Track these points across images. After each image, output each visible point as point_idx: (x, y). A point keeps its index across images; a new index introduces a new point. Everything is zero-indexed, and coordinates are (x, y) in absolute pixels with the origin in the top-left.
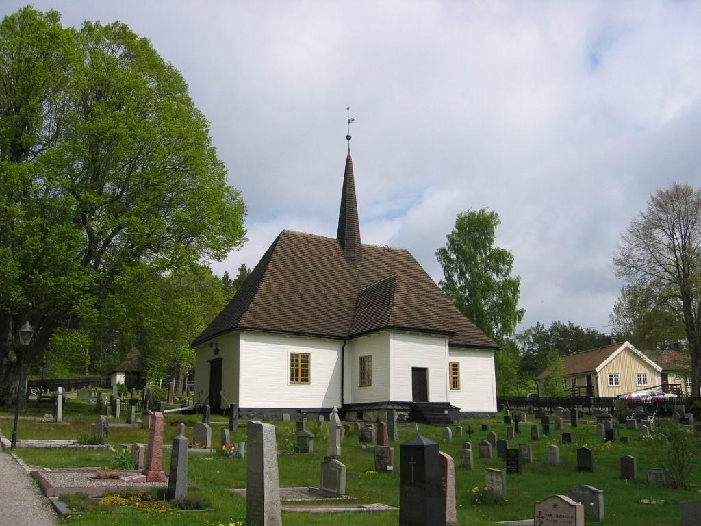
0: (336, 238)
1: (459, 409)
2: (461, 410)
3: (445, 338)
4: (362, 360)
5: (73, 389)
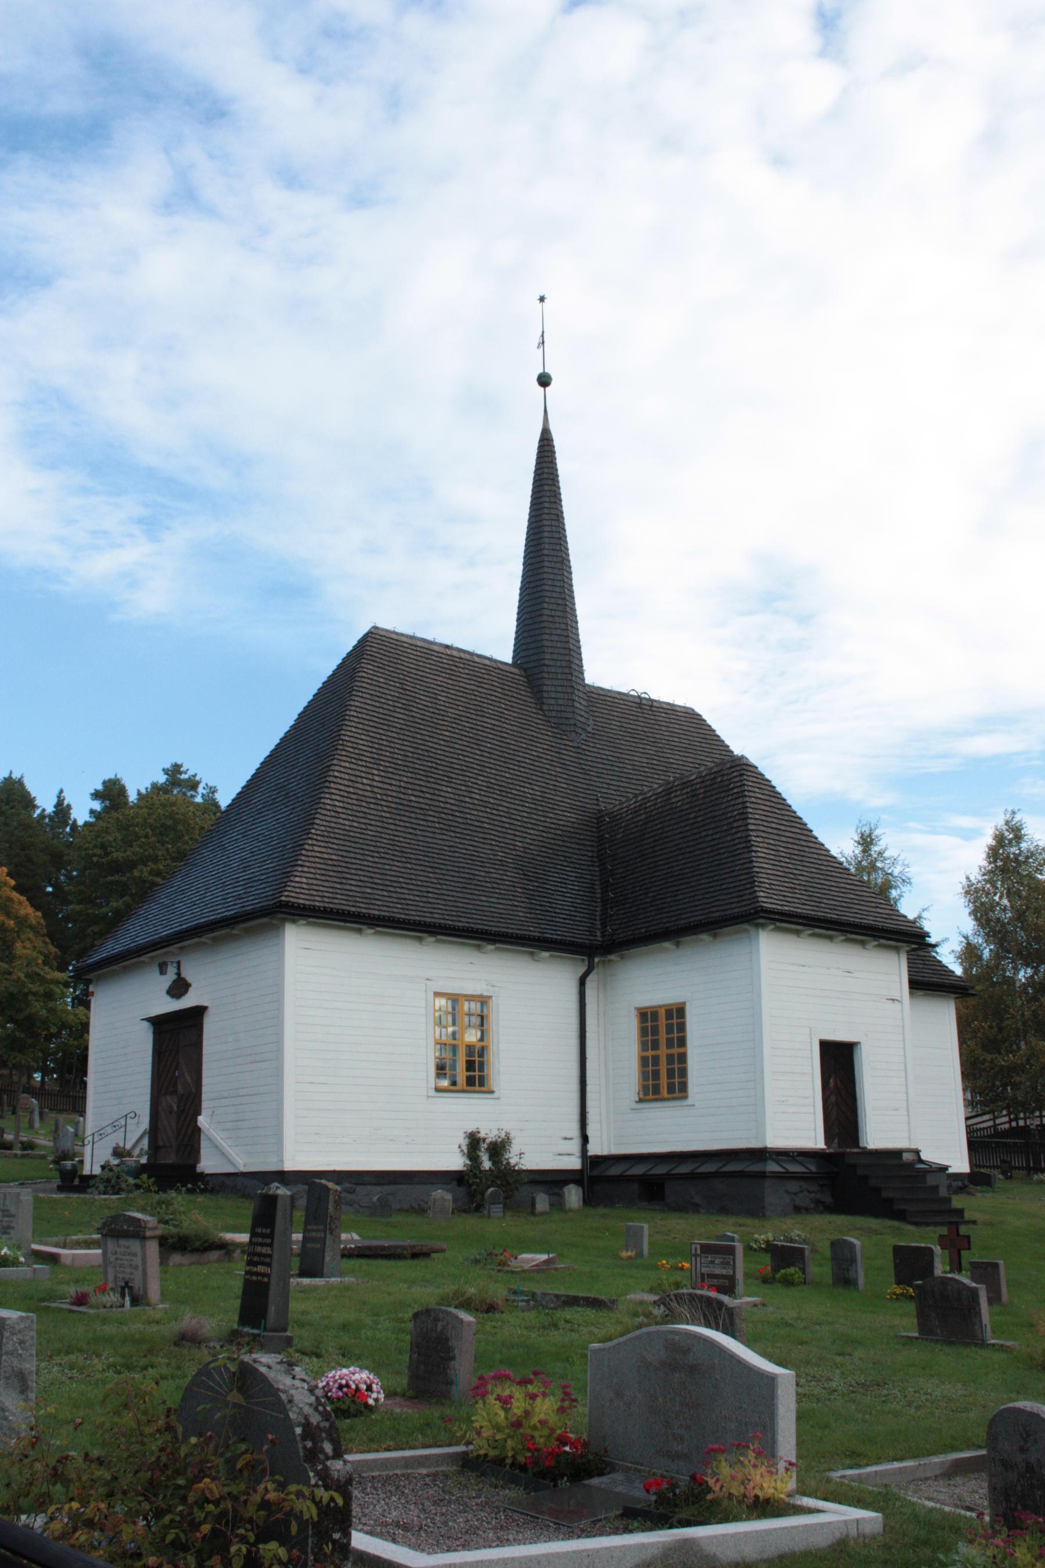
0: (509, 660)
1: (946, 1168)
2: (950, 1171)
3: (897, 949)
4: (647, 1017)
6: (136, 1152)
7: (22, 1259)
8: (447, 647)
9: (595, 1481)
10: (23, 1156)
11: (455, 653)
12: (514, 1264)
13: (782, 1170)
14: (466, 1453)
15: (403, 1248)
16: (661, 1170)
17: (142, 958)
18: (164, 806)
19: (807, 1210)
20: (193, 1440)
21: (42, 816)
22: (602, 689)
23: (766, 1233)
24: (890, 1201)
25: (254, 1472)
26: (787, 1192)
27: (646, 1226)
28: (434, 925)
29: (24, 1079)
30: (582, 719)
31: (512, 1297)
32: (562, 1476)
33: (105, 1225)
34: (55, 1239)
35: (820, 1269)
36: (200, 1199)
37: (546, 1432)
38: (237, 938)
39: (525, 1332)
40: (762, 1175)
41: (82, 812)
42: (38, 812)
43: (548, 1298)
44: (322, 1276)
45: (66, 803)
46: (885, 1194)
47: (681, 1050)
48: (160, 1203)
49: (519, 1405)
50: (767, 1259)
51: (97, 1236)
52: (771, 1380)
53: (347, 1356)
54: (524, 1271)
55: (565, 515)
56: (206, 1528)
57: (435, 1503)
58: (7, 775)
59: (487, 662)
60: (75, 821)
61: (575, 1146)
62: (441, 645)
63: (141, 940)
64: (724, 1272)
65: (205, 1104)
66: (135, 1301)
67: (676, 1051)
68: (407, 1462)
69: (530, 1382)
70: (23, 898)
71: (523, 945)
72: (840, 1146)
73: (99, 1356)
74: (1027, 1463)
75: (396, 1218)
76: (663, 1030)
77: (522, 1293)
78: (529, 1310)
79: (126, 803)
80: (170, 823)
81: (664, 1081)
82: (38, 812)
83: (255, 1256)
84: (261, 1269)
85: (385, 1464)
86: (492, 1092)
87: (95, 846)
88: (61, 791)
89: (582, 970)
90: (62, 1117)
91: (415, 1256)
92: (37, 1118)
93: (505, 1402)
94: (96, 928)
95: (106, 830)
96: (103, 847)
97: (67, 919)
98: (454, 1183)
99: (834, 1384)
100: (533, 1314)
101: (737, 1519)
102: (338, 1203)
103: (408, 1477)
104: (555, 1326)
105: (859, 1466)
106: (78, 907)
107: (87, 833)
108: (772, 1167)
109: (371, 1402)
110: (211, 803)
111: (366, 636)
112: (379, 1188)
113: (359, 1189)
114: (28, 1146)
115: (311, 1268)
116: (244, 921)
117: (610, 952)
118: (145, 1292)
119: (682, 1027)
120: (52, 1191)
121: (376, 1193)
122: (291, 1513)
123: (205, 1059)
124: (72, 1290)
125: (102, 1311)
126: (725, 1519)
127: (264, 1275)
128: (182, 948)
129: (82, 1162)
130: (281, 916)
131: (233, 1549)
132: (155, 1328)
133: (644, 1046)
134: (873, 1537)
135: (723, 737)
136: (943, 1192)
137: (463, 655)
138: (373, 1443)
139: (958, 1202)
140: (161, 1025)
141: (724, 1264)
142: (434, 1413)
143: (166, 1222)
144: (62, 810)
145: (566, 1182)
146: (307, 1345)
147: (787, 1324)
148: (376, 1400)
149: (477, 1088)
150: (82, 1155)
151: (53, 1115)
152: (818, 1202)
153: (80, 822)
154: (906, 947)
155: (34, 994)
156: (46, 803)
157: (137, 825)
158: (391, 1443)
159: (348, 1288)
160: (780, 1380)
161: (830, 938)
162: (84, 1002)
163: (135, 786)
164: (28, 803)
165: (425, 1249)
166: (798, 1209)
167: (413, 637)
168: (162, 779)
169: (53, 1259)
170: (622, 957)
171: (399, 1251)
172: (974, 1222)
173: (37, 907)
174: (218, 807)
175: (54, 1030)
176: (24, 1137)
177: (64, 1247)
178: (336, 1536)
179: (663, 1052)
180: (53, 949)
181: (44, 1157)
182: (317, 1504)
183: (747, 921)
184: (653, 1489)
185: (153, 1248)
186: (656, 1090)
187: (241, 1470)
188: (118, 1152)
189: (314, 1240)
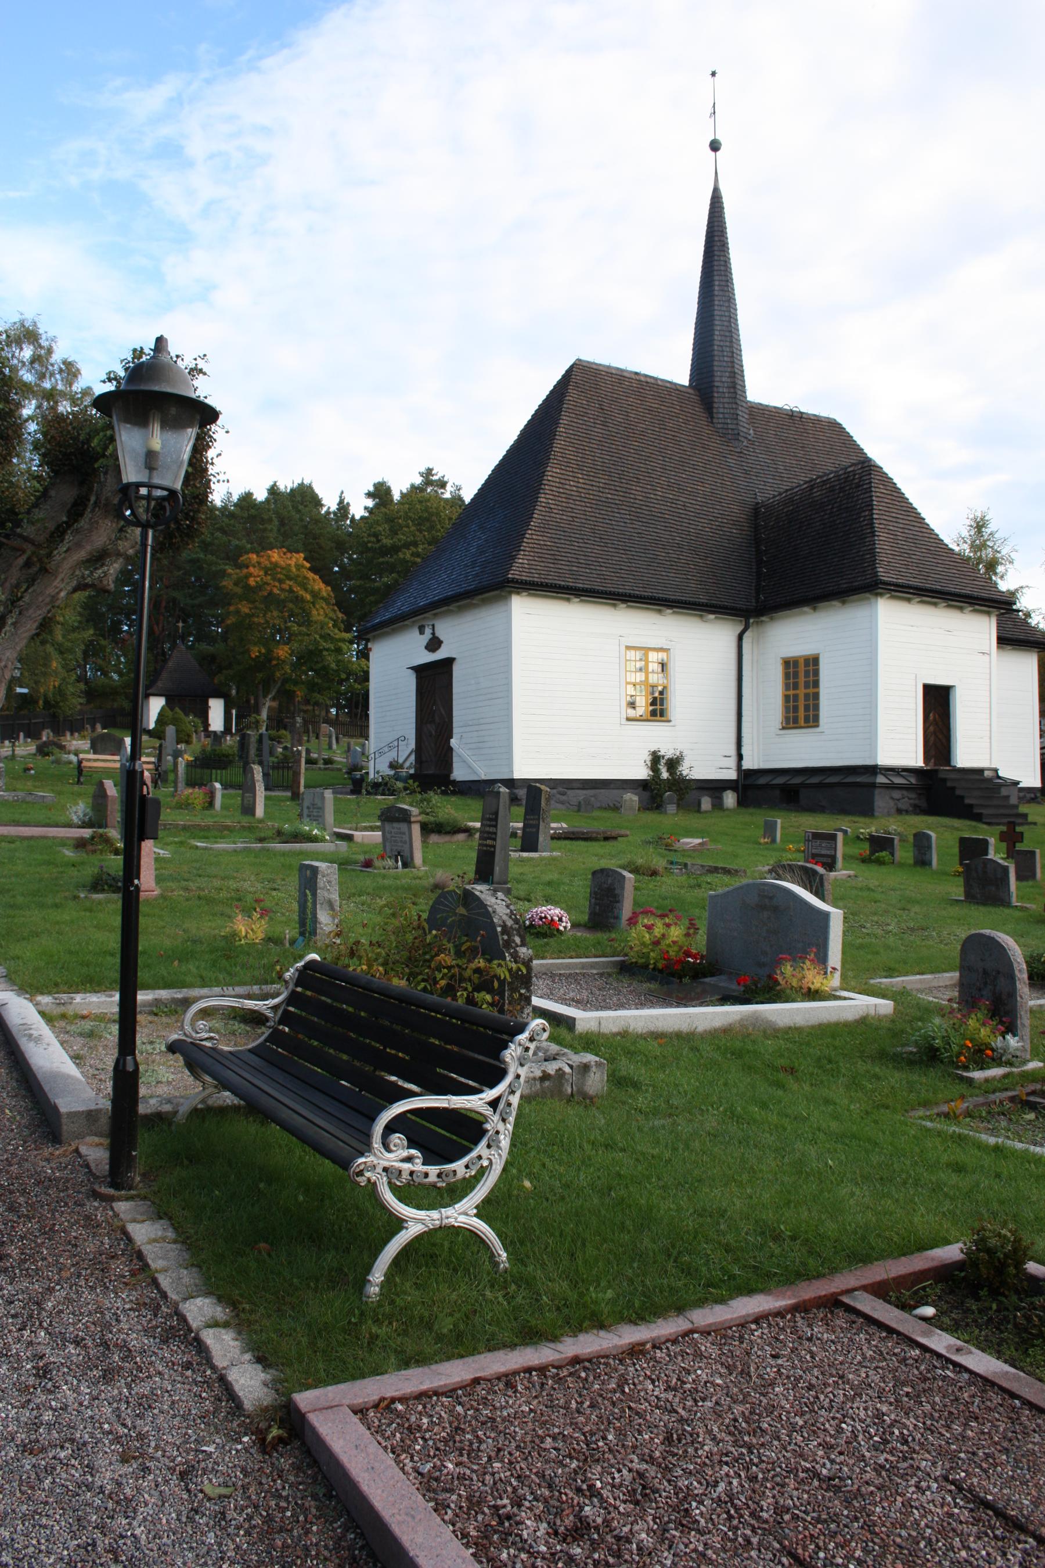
0: (687, 384)
1: (1018, 783)
2: (1021, 785)
3: (988, 613)
4: (790, 666)
5: (68, 734)
6: (407, 764)
7: (327, 838)
8: (636, 373)
9: (707, 980)
10: (326, 769)
11: (643, 379)
12: (677, 846)
13: (888, 781)
14: (624, 961)
15: (598, 833)
16: (797, 780)
17: (406, 623)
18: (420, 502)
19: (907, 812)
20: (434, 932)
21: (328, 513)
22: (761, 404)
23: (869, 828)
24: (971, 806)
25: (473, 953)
26: (892, 798)
27: (779, 821)
28: (625, 595)
29: (323, 713)
30: (745, 430)
31: (669, 866)
32: (685, 976)
33: (382, 814)
34: (349, 826)
35: (904, 853)
36: (453, 799)
37: (676, 948)
38: (475, 606)
39: (677, 889)
40: (873, 785)
41: (359, 507)
42: (325, 509)
43: (696, 867)
44: (536, 851)
45: (346, 502)
46: (967, 801)
47: (815, 690)
48: (422, 801)
49: (658, 931)
50: (866, 846)
51: (378, 824)
52: (826, 916)
53: (548, 900)
54: (684, 850)
55: (732, 261)
56: (443, 983)
57: (600, 990)
58: (300, 482)
59: (668, 385)
60: (353, 516)
61: (732, 762)
62: (631, 372)
63: (406, 608)
64: (828, 852)
65: (455, 731)
66: (405, 865)
67: (811, 690)
68: (583, 966)
69: (666, 915)
70: (317, 577)
71: (694, 609)
72: (935, 765)
73: (381, 898)
74: (984, 970)
75: (596, 813)
76: (802, 675)
77: (677, 863)
78: (682, 875)
79: (392, 500)
80: (425, 515)
81: (801, 713)
82: (325, 509)
83: (489, 833)
84: (489, 842)
85: (568, 966)
86: (669, 721)
87: (369, 535)
88: (342, 493)
89: (740, 628)
90: (352, 741)
91: (606, 839)
92: (334, 741)
93: (649, 928)
94: (372, 598)
95: (377, 523)
96: (376, 535)
97: (350, 591)
98: (641, 789)
99: (890, 928)
100: (685, 877)
101: (793, 1001)
102: (548, 800)
103: (584, 975)
104: (699, 886)
105: (892, 977)
106: (358, 583)
107: (362, 525)
108: (881, 779)
109: (561, 928)
110: (457, 499)
111: (572, 367)
112: (584, 792)
113: (569, 792)
114: (328, 762)
115: (529, 843)
116: (481, 594)
117: (762, 615)
118: (412, 858)
119: (816, 673)
120: (347, 794)
121: (582, 794)
122: (495, 976)
123: (454, 697)
124: (361, 858)
125: (383, 871)
126: (787, 1001)
127: (491, 846)
128: (435, 615)
129: (367, 773)
130: (508, 589)
131: (459, 994)
132: (418, 881)
133: (787, 686)
134: (886, 1016)
135: (859, 442)
136: (1013, 800)
137: (649, 380)
138: (560, 954)
139: (1023, 809)
140: (421, 671)
141: (829, 849)
142: (602, 936)
143: (427, 814)
144: (343, 508)
145: (725, 789)
146: (522, 894)
147: (869, 889)
148: (565, 927)
149: (658, 718)
150: (368, 768)
151: (346, 739)
152: (915, 806)
153: (357, 517)
154: (996, 612)
155: (327, 650)
156: (330, 503)
157: (400, 518)
158: (573, 954)
159: (554, 859)
160: (832, 916)
161: (935, 604)
162: (364, 654)
163: (397, 491)
164: (317, 502)
165: (613, 835)
166: (899, 811)
167: (609, 367)
168: (418, 480)
169: (349, 838)
170: (772, 619)
171: (594, 835)
172: (1035, 824)
173: (327, 583)
174: (463, 501)
175: (344, 676)
176: (325, 755)
177: (356, 830)
178: (523, 991)
179: (801, 692)
180: (340, 615)
181: (340, 770)
182: (510, 971)
183: (869, 591)
184: (742, 983)
185: (416, 829)
186: (796, 720)
187: (464, 952)
188: (393, 766)
189: (531, 826)
